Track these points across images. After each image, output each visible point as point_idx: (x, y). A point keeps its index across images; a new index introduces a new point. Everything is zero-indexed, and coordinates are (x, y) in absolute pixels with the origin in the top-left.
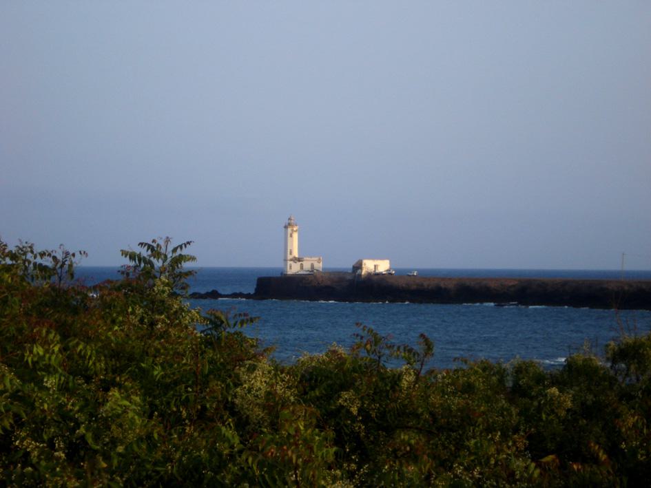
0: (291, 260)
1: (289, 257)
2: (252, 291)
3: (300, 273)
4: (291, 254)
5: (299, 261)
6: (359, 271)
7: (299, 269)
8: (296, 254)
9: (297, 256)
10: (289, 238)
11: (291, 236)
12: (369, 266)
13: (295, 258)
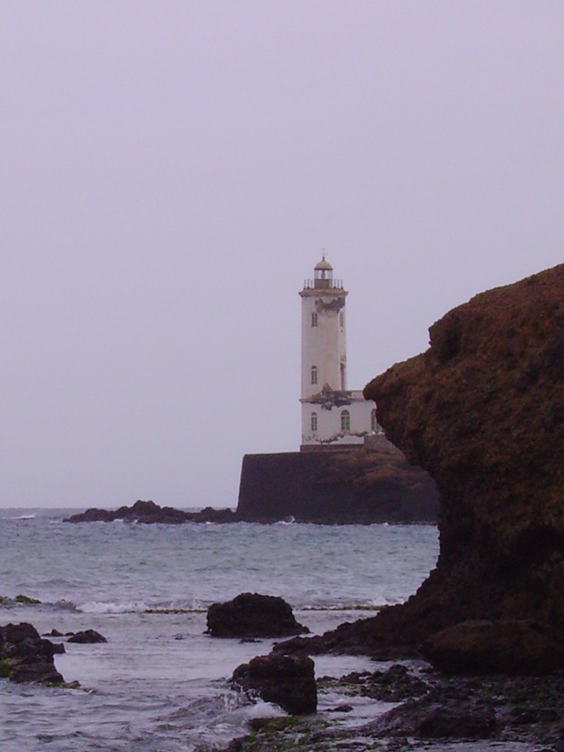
3: (340, 441)
13: (327, 390)
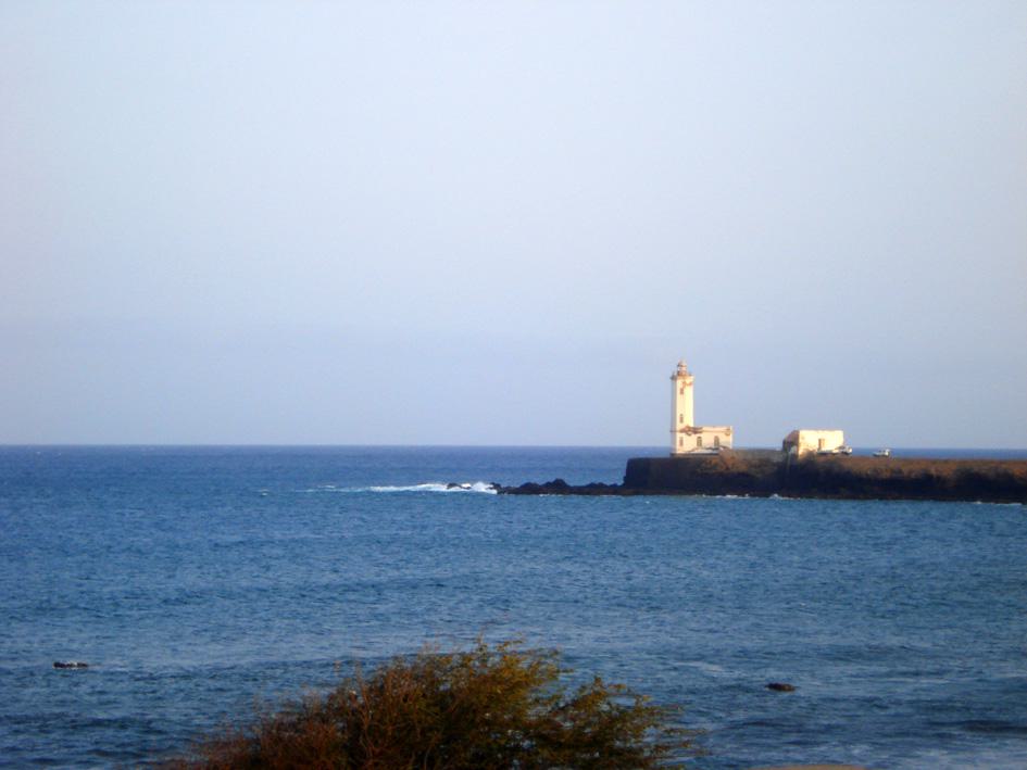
0: (682, 431)
1: (679, 426)
2: (620, 483)
3: (696, 452)
4: (682, 421)
5: (695, 433)
6: (793, 449)
7: (695, 445)
8: (689, 422)
9: (692, 425)
10: (679, 396)
11: (682, 392)
12: (809, 442)
13: (688, 427)
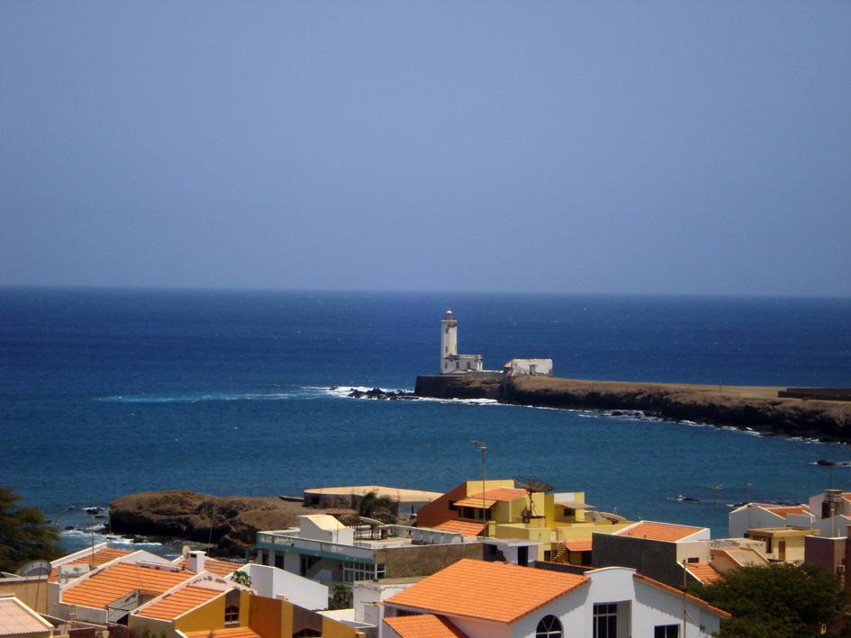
6: (509, 372)
9: (455, 353)
11: (447, 332)
